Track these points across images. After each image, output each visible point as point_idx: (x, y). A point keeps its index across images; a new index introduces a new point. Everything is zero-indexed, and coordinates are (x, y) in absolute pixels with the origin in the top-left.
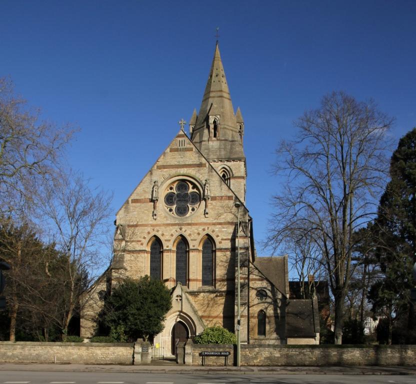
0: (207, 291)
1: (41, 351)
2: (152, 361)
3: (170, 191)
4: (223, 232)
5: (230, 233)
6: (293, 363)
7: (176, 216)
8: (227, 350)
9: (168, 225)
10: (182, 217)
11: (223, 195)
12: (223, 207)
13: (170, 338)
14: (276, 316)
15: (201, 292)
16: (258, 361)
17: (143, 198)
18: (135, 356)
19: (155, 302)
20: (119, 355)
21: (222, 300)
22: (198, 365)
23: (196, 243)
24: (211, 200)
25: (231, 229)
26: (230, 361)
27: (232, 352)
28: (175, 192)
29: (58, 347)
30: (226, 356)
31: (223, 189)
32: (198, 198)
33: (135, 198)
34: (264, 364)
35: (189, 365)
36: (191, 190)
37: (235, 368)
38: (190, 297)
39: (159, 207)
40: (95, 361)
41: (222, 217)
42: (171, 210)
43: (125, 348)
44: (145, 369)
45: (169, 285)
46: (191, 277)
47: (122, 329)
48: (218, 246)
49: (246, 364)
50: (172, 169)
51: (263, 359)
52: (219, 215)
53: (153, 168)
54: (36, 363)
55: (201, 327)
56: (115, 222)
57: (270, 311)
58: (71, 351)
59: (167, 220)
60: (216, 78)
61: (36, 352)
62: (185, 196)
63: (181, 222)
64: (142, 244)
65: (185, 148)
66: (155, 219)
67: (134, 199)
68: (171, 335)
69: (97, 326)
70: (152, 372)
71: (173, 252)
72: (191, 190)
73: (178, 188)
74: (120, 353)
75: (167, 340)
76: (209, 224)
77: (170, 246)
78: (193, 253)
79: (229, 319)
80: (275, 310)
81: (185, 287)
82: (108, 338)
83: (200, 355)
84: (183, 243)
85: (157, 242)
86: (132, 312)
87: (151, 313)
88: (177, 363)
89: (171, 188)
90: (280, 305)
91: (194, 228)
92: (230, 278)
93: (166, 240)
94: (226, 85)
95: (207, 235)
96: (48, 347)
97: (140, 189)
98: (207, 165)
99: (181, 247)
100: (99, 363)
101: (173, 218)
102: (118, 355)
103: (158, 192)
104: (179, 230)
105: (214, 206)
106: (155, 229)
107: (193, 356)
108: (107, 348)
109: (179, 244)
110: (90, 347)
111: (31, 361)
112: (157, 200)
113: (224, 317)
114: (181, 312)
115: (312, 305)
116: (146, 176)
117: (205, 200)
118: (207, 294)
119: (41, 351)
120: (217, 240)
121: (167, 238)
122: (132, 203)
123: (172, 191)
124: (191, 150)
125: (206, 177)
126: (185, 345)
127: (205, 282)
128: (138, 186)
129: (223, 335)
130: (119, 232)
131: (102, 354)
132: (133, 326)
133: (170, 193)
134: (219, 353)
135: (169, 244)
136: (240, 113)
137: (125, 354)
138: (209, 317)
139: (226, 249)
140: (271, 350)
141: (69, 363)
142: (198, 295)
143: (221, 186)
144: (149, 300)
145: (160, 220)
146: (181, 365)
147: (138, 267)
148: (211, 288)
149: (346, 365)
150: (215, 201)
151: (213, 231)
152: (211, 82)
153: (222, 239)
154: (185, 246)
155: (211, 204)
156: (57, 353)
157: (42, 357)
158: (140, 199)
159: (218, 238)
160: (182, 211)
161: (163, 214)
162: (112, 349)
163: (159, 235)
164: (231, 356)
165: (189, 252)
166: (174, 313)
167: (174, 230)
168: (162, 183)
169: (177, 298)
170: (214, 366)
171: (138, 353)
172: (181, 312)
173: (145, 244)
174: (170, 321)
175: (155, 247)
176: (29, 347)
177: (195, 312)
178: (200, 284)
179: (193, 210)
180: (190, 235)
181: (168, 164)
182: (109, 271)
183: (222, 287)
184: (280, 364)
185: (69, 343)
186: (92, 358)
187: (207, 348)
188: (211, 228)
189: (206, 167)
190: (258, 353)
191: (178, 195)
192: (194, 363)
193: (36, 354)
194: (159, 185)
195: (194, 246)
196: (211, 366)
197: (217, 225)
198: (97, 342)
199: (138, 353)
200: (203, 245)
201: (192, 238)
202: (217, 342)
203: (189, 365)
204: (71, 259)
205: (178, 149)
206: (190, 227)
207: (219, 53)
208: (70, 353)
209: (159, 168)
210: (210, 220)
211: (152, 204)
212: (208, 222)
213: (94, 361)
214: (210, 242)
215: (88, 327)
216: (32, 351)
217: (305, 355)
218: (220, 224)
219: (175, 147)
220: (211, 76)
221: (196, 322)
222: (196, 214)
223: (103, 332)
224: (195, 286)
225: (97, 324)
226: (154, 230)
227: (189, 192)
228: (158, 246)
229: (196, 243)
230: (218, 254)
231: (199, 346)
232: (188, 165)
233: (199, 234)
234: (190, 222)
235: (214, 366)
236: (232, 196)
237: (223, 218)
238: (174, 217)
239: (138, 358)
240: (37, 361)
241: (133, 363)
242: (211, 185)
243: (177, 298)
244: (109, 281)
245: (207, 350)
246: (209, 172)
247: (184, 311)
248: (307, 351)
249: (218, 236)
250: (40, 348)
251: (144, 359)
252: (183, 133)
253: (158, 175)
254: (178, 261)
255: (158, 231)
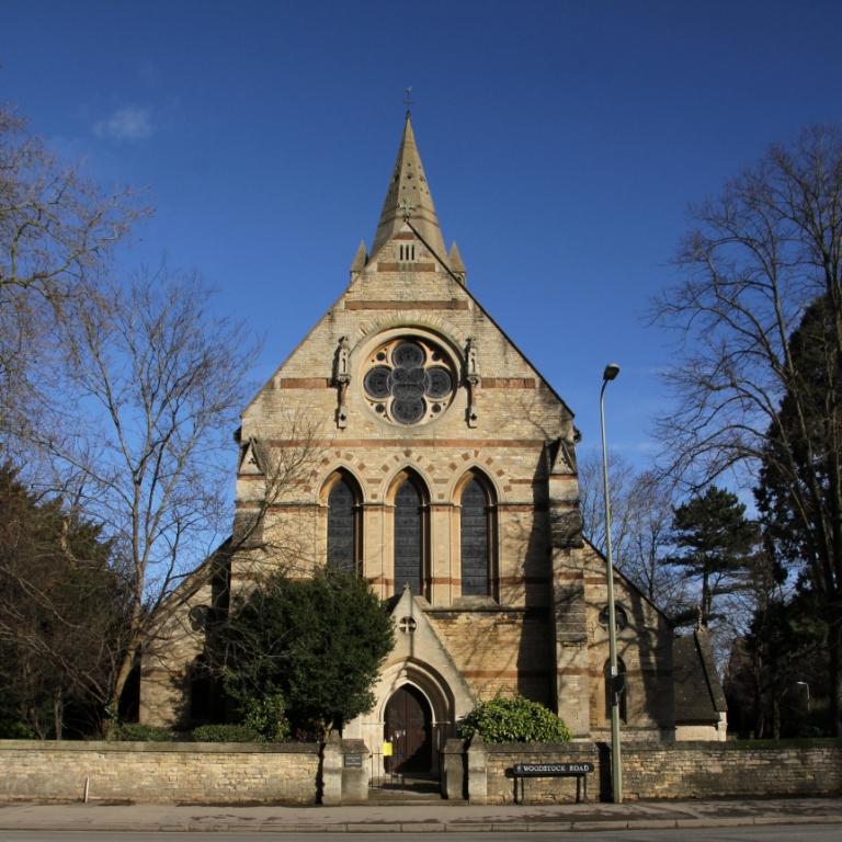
0: (474, 608)
1: (44, 767)
2: (371, 793)
3: (377, 363)
4: (513, 463)
5: (529, 469)
6: (756, 789)
7: (394, 422)
8: (583, 758)
9: (376, 443)
10: (413, 426)
11: (511, 375)
12: (507, 405)
13: (382, 729)
14: (646, 672)
15: (460, 611)
16: (666, 786)
17: (310, 375)
18: (326, 778)
19: (358, 631)
20: (277, 777)
21: (511, 635)
22: (504, 803)
23: (444, 488)
24: (482, 387)
25: (531, 459)
26: (593, 788)
27: (596, 763)
28: (390, 364)
29: (96, 755)
30: (579, 775)
31: (510, 361)
32: (455, 378)
33: (291, 376)
34: (682, 795)
35: (480, 804)
36: (430, 362)
37: (603, 807)
38: (434, 624)
39: (350, 399)
40: (207, 795)
41: (510, 427)
42: (380, 409)
43: (295, 757)
44: (378, 818)
45: (382, 592)
46: (436, 572)
47: (278, 704)
48: (503, 497)
49: (633, 796)
50: (383, 311)
51: (677, 779)
52: (500, 424)
53: (337, 308)
54: (29, 800)
55: (468, 700)
56: (238, 436)
57: (633, 658)
58: (136, 766)
59: (372, 431)
60: (408, 182)
61: (29, 771)
62: (416, 374)
63: (407, 437)
64: (308, 489)
65: (416, 264)
66: (343, 428)
67: (289, 379)
68: (383, 722)
69: (183, 699)
70: (405, 827)
71: (388, 512)
72: (430, 362)
73: (400, 356)
74: (281, 772)
75: (375, 734)
76: (479, 443)
77: (380, 494)
78: (439, 513)
79: (539, 678)
80: (644, 655)
81: (421, 599)
82: (240, 728)
83: (510, 773)
84: (413, 485)
85: (345, 486)
86: (282, 659)
87: (350, 659)
88: (445, 796)
89: (381, 357)
90: (654, 644)
91: (440, 452)
92: (538, 575)
93: (370, 481)
94: (429, 196)
95: (475, 470)
96: (67, 754)
97: (301, 356)
98: (471, 304)
99: (408, 500)
100: (217, 799)
101: (388, 427)
102: (272, 777)
103: (350, 363)
104: (403, 455)
105: (489, 400)
106: (342, 453)
107: (490, 777)
108: (241, 756)
109: (401, 491)
110: (191, 756)
111: (13, 796)
112: (347, 382)
113: (521, 675)
114: (410, 659)
115: (697, 645)
116: (318, 324)
117: (468, 386)
118: (474, 617)
119: (44, 767)
120: (499, 483)
121: (373, 474)
122: (282, 387)
123: (383, 363)
124: (430, 268)
125: (469, 333)
126: (467, 746)
127: (468, 587)
128: (298, 348)
129: (538, 720)
130: (249, 456)
131: (226, 774)
132: (305, 698)
133: (377, 367)
134: (563, 769)
135: (378, 488)
136: (457, 254)
137: (294, 774)
138: (478, 674)
139: (521, 506)
140: (699, 756)
141: (129, 803)
142: (455, 617)
143: (505, 354)
144: (343, 628)
145: (354, 430)
146: (456, 803)
147: (299, 543)
148: (488, 602)
149: (50, 801)
150: (492, 390)
151: (489, 461)
152: (397, 189)
153: (512, 481)
154: (416, 496)
155: (483, 396)
156: (94, 772)
157: (48, 784)
158: (303, 379)
159: (501, 478)
160: (408, 412)
161: (363, 418)
162: (255, 759)
163: (352, 466)
164: (594, 777)
165: (428, 510)
166: (394, 663)
167: (390, 457)
168: (359, 341)
169: (402, 625)
170: (546, 803)
171: (333, 772)
172: (410, 659)
173: (316, 490)
174: (387, 682)
175: (340, 497)
176: (10, 754)
177: (450, 661)
178: (457, 592)
179: (436, 409)
180: (431, 468)
181: (373, 299)
182: (228, 550)
183: (516, 598)
184: (722, 794)
185: (127, 744)
186: (199, 786)
187: (527, 754)
188: (485, 453)
189: (466, 308)
190: (663, 765)
191: (398, 374)
192: (493, 797)
193: (29, 775)
194: (352, 347)
195: (441, 496)
196: (540, 803)
197: (499, 445)
198: (210, 740)
199: (333, 772)
200: (463, 495)
201: (436, 476)
202: (522, 739)
203: (480, 804)
204: (102, 540)
205: (398, 264)
206: (430, 449)
207: (412, 134)
208: (131, 772)
209: (351, 306)
210: (482, 433)
211: (335, 391)
212: (476, 437)
213: (201, 796)
214: (478, 488)
215: (160, 701)
216: (17, 767)
217: (785, 766)
218: (506, 444)
219: (392, 260)
220: (397, 178)
221: (455, 687)
222: (446, 418)
223: (208, 710)
224: (444, 596)
225: (185, 693)
226: (338, 454)
227: (426, 366)
228: (347, 497)
229: (444, 488)
230: (503, 517)
231: (505, 749)
232: (424, 303)
233: (453, 467)
234: (430, 437)
235: (546, 803)
236: (533, 380)
237: (513, 431)
238: (391, 425)
239: (332, 784)
240: (33, 795)
241: (318, 800)
242: (482, 351)
243: (402, 625)
244: (220, 582)
245: (526, 760)
246: (475, 321)
247: (417, 655)
248: (789, 758)
249: (500, 473)
250: (42, 757)
251: (349, 786)
252: (409, 230)
253: (347, 324)
254: (399, 532)
255: (349, 457)
